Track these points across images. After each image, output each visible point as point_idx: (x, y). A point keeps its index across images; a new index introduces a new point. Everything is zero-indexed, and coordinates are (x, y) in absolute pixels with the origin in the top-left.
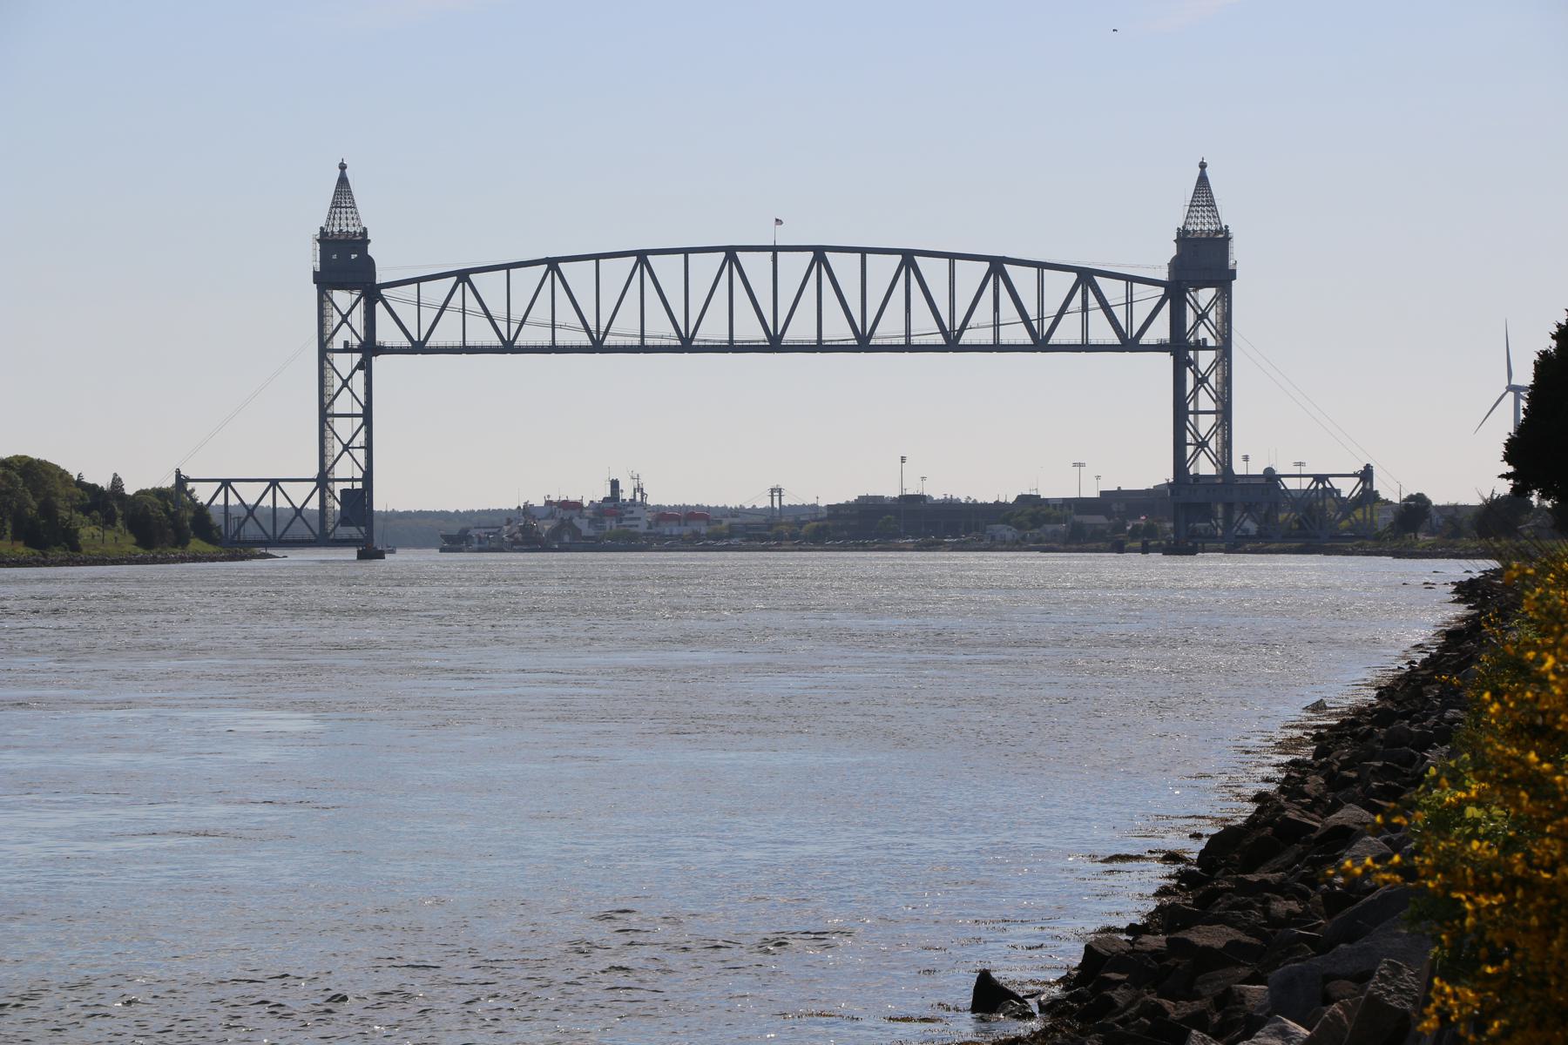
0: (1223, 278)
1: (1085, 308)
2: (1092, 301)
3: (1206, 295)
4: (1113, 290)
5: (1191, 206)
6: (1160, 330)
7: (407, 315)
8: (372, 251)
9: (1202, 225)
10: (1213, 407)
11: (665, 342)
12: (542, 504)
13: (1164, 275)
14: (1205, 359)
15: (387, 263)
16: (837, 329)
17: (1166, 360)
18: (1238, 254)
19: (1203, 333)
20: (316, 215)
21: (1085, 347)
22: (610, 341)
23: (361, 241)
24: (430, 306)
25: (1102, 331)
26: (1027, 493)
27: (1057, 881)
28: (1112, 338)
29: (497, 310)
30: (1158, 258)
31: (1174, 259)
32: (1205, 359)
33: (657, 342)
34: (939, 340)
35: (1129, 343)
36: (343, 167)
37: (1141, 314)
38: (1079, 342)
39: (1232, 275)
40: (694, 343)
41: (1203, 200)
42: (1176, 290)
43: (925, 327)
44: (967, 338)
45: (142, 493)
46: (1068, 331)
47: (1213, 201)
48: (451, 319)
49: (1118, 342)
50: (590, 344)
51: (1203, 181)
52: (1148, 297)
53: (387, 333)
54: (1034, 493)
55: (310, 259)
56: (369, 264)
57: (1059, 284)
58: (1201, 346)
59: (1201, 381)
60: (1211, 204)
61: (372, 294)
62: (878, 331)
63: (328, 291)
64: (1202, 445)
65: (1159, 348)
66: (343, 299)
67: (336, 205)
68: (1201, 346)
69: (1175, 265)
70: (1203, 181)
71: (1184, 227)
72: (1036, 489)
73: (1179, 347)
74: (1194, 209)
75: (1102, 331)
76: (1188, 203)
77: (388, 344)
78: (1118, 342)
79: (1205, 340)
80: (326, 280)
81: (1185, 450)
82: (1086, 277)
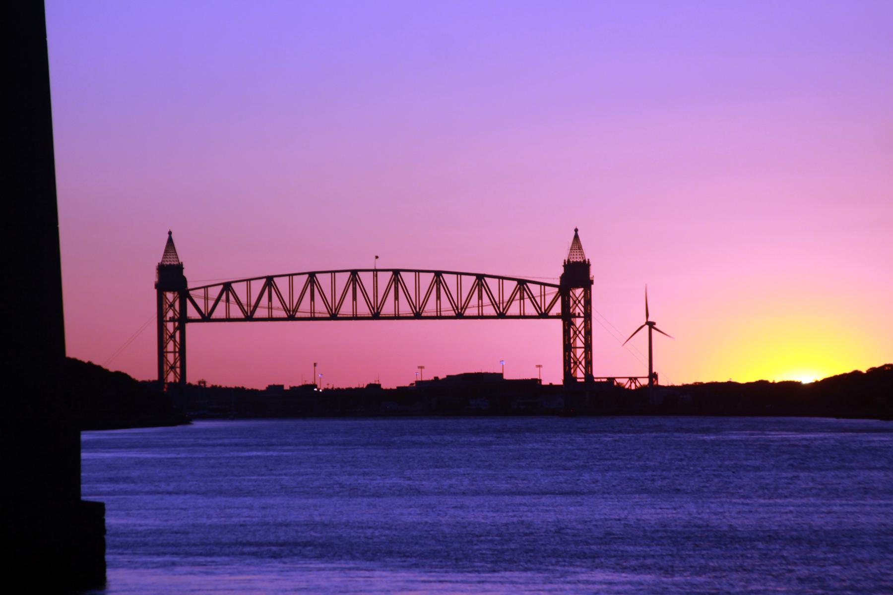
0: (587, 284)
1: (228, 300)
2: (231, 298)
3: (579, 292)
4: (535, 289)
5: (571, 250)
6: (557, 309)
7: (201, 303)
8: (186, 273)
9: (170, 261)
10: (583, 346)
11: (324, 316)
12: (396, 388)
13: (558, 283)
14: (579, 322)
15: (193, 277)
16: (405, 308)
17: (559, 323)
18: (594, 272)
19: (577, 311)
20: (157, 257)
21: (228, 319)
22: (298, 315)
23: (180, 267)
24: (212, 299)
25: (530, 310)
26: (373, 382)
27: (616, 536)
28: (240, 315)
29: (243, 300)
30: (555, 274)
31: (563, 275)
32: (579, 322)
33: (320, 315)
34: (452, 313)
35: (544, 315)
36: (576, 230)
37: (549, 299)
38: (267, 317)
39: (592, 282)
40: (338, 316)
41: (576, 247)
42: (564, 289)
43: (446, 307)
44: (468, 312)
45: (867, 371)
46: (514, 310)
47: (581, 247)
48: (222, 305)
49: (200, 318)
50: (537, 314)
51: (576, 237)
52: (551, 292)
53: (192, 312)
54: (377, 383)
55: (154, 278)
56: (184, 281)
57: (510, 286)
58: (172, 320)
59: (172, 336)
60: (580, 248)
61: (184, 294)
62: (382, 311)
63: (164, 293)
64: (173, 368)
65: (556, 317)
66: (170, 296)
67: (166, 251)
68: (172, 320)
69: (563, 278)
70: (576, 237)
71: (161, 263)
72: (378, 381)
73: (567, 317)
74: (573, 251)
75: (530, 310)
76: (570, 248)
77: (193, 318)
78: (200, 318)
79: (579, 314)
80: (161, 287)
81: (571, 365)
82: (522, 284)
